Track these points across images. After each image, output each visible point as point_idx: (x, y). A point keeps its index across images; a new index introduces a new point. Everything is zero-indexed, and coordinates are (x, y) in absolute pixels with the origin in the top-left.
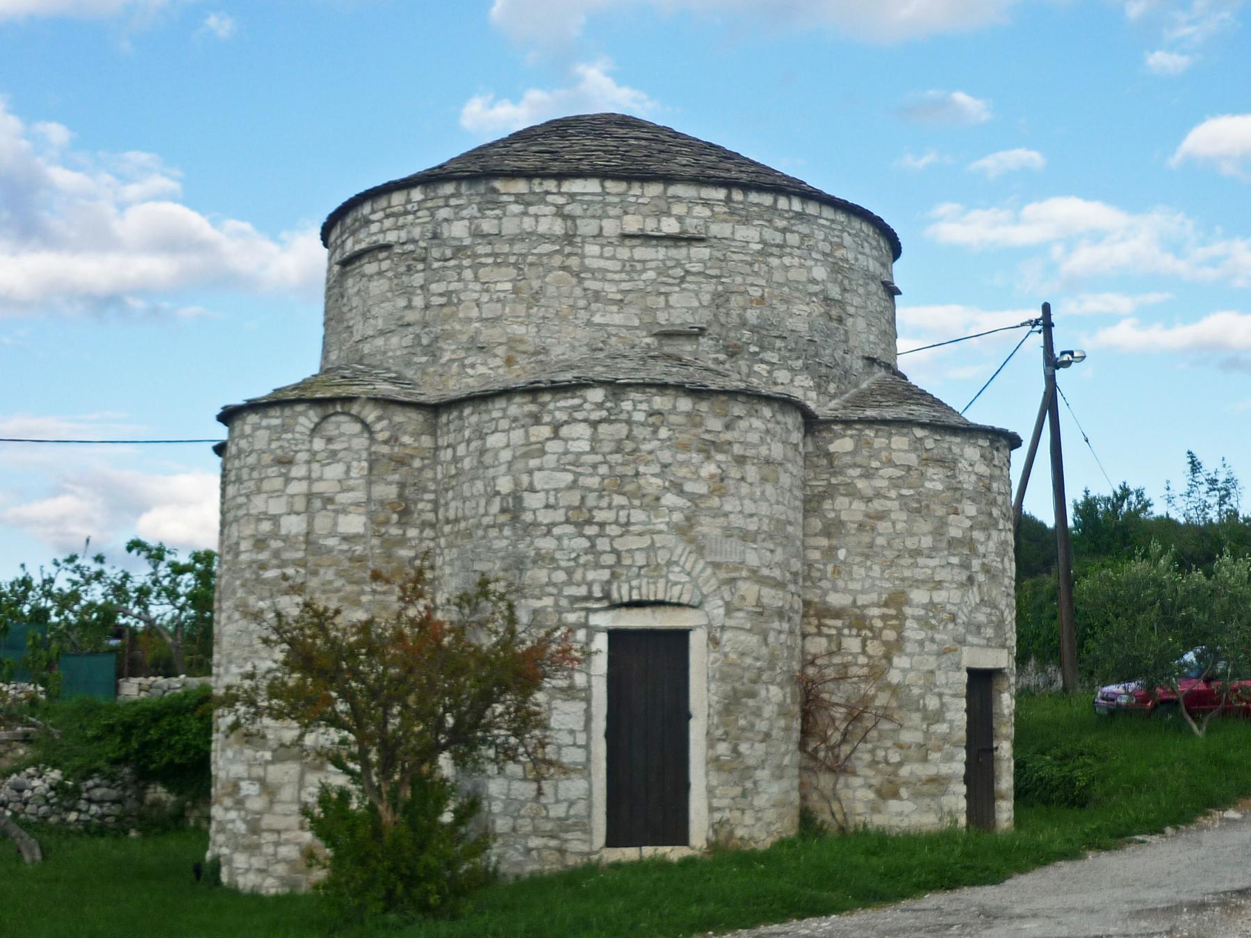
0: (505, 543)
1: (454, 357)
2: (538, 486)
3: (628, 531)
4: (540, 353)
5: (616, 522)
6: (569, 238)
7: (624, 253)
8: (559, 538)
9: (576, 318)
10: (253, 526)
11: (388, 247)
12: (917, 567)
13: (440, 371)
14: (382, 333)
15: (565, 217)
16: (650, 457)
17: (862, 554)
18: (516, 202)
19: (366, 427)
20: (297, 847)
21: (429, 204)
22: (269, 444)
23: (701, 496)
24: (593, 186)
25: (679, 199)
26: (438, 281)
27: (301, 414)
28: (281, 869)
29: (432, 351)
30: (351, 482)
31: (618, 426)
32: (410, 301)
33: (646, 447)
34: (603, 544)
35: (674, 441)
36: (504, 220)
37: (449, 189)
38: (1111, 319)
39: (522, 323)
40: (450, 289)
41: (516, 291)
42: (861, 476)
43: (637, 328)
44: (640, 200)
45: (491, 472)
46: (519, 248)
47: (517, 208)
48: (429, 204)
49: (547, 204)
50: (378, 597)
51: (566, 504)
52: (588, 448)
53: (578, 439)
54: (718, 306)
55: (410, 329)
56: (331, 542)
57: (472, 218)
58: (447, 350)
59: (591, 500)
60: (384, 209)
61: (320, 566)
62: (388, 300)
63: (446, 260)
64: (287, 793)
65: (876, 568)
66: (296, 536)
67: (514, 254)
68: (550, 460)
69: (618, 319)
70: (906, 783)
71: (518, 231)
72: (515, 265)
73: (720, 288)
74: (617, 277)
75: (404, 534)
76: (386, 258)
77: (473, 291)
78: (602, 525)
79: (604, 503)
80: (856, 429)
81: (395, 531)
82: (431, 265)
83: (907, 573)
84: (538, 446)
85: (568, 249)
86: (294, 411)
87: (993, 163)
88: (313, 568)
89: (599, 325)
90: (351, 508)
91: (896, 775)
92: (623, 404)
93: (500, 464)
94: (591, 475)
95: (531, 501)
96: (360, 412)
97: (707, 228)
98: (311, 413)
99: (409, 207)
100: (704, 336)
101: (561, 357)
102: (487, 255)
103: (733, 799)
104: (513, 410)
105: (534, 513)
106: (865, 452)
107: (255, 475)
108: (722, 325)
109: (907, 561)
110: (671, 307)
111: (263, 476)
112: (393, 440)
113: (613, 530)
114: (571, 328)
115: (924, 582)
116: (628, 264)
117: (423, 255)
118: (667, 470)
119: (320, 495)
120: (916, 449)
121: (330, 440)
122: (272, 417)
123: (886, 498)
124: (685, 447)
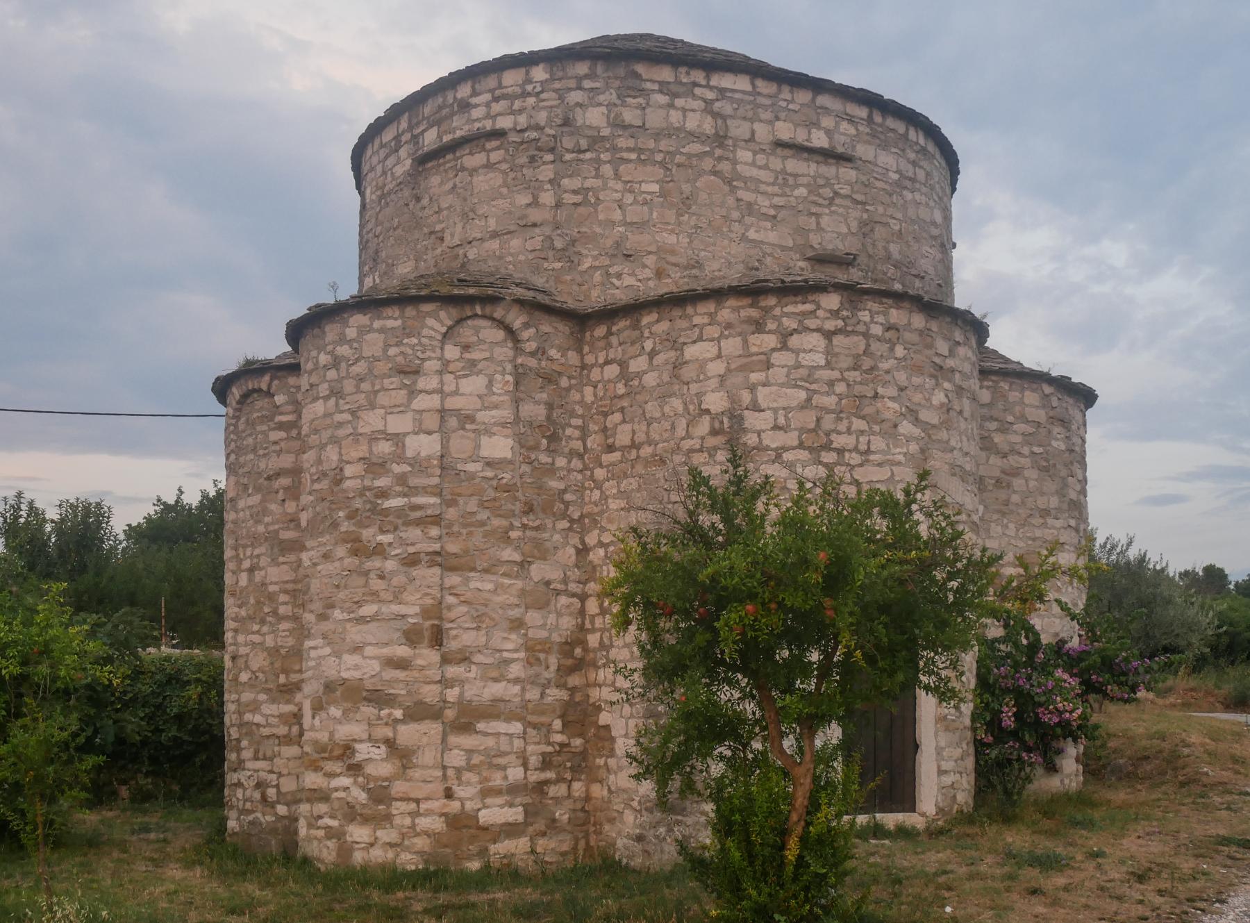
1: (597, 263)
2: (763, 403)
3: (867, 461)
4: (694, 267)
5: (856, 449)
6: (720, 139)
7: (776, 163)
9: (731, 231)
10: (365, 448)
11: (499, 134)
13: (579, 279)
14: (495, 235)
15: (716, 115)
16: (888, 377)
17: (999, 511)
18: (661, 92)
19: (510, 331)
20: (443, 819)
21: (557, 85)
22: (385, 351)
23: (934, 426)
26: (571, 176)
27: (428, 314)
28: (421, 843)
29: (568, 254)
30: (495, 398)
31: (856, 338)
32: (535, 198)
33: (884, 365)
35: (909, 362)
36: (648, 110)
39: (672, 231)
40: (585, 186)
41: (663, 194)
42: (997, 430)
43: (791, 249)
44: (791, 106)
45: (694, 388)
46: (664, 144)
47: (662, 99)
48: (557, 85)
49: (694, 97)
50: (528, 533)
51: (799, 425)
52: (823, 363)
53: (811, 351)
54: (865, 235)
55: (537, 230)
56: (472, 467)
57: (610, 105)
58: (587, 256)
59: (828, 422)
60: (492, 91)
61: (460, 495)
62: (503, 197)
64: (428, 757)
65: (1011, 526)
66: (429, 458)
67: (661, 151)
68: (778, 374)
69: (772, 237)
71: (664, 125)
72: (662, 164)
73: (865, 216)
74: (770, 189)
75: (553, 464)
76: (498, 148)
77: (611, 195)
78: (840, 451)
79: (842, 427)
80: (993, 381)
81: (544, 458)
83: (1038, 533)
84: (762, 357)
85: (718, 152)
86: (418, 311)
88: (449, 497)
89: (753, 241)
90: (495, 429)
92: (860, 314)
94: (828, 394)
95: (753, 420)
97: (854, 147)
98: (442, 314)
99: (529, 88)
100: (853, 267)
101: (716, 273)
102: (629, 150)
103: (956, 761)
104: (725, 314)
105: (759, 435)
106: (1000, 405)
107: (365, 386)
108: (870, 256)
109: (1037, 521)
110: (823, 229)
111: (377, 387)
112: (539, 353)
114: (726, 242)
116: (780, 177)
117: (552, 144)
118: (902, 394)
120: (1044, 407)
121: (466, 347)
122: (389, 318)
124: (918, 370)
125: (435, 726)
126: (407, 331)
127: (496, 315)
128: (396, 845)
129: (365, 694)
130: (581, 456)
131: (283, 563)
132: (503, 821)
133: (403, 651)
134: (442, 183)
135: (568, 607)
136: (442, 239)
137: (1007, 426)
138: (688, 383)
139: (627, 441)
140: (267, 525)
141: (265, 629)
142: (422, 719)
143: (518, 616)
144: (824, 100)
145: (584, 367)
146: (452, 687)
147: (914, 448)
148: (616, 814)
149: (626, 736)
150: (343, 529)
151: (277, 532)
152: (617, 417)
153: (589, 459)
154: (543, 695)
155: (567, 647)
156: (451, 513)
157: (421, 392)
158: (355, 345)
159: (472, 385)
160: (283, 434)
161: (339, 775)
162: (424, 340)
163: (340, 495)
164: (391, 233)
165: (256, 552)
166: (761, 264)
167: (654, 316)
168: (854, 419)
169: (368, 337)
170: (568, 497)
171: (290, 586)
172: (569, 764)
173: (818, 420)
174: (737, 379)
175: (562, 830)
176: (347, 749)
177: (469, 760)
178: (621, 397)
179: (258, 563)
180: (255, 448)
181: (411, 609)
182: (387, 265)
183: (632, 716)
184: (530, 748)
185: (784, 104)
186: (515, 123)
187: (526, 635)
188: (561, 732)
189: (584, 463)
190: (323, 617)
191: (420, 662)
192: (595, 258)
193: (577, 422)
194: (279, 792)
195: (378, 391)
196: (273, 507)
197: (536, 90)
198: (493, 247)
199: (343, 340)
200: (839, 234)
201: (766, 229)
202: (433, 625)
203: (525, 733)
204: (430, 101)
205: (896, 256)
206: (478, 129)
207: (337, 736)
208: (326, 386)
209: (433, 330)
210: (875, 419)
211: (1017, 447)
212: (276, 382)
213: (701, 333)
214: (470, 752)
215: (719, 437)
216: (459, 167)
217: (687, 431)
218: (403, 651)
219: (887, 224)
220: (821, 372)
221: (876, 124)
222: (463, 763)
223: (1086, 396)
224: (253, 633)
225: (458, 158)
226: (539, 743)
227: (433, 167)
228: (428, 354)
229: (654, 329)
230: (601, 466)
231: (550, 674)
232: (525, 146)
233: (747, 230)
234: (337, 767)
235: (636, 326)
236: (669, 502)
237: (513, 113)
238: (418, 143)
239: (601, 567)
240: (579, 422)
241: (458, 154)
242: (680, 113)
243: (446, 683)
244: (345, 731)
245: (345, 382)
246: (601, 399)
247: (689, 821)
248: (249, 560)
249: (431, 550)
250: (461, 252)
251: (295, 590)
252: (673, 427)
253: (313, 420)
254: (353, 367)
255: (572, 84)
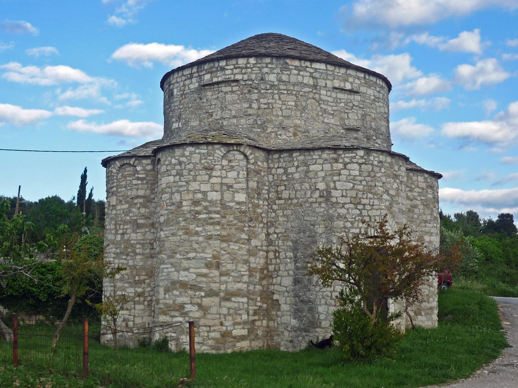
0: (322, 210)
1: (273, 130)
5: (369, 204)
6: (315, 86)
7: (334, 95)
8: (348, 209)
10: (192, 195)
11: (237, 81)
12: (426, 227)
13: (266, 135)
14: (235, 117)
15: (314, 78)
16: (379, 179)
18: (295, 69)
19: (246, 156)
21: (259, 66)
22: (200, 161)
23: (394, 196)
24: (322, 66)
25: (351, 75)
26: (263, 98)
27: (217, 149)
29: (263, 127)
32: (250, 105)
33: (378, 175)
34: (365, 213)
36: (291, 76)
37: (268, 60)
38: (76, 118)
39: (299, 119)
40: (269, 102)
41: (296, 106)
43: (339, 125)
45: (313, 180)
46: (296, 88)
47: (296, 72)
48: (259, 66)
50: (251, 229)
52: (358, 174)
53: (354, 170)
54: (363, 120)
55: (251, 117)
56: (232, 204)
58: (269, 127)
59: (360, 195)
60: (234, 65)
61: (227, 214)
63: (267, 90)
64: (214, 310)
66: (216, 201)
68: (343, 177)
69: (332, 121)
70: (424, 310)
71: (296, 81)
72: (295, 95)
73: (363, 113)
74: (332, 104)
75: (259, 203)
77: (278, 105)
78: (364, 205)
79: (365, 196)
81: (256, 201)
82: (260, 91)
83: (423, 229)
84: (338, 171)
85: (314, 91)
86: (213, 148)
87: (35, 51)
89: (326, 123)
90: (240, 191)
91: (420, 306)
92: (370, 157)
93: (318, 178)
94: (360, 185)
95: (334, 193)
96: (244, 151)
98: (222, 149)
99: (248, 66)
100: (360, 131)
102: (284, 90)
104: (325, 155)
105: (337, 199)
107: (192, 173)
109: (423, 225)
110: (349, 118)
111: (197, 174)
112: (255, 163)
113: (368, 207)
115: (428, 233)
118: (384, 185)
119: (226, 184)
120: (425, 182)
121: (230, 161)
122: (202, 149)
123: (417, 199)
124: (388, 176)
125: (217, 299)
126: (209, 154)
127: (241, 150)
128: (201, 343)
129: (189, 286)
130: (267, 200)
131: (139, 232)
132: (241, 334)
133: (205, 271)
134: (212, 95)
135: (262, 255)
136: (212, 115)
137: (412, 189)
138: (311, 179)
139: (287, 197)
140: (131, 217)
141: (129, 258)
142: (212, 296)
143: (247, 258)
144: (350, 72)
145: (269, 168)
146: (223, 284)
147: (387, 203)
148: (280, 333)
149: (286, 303)
150: (181, 225)
151: (136, 220)
152: (283, 188)
153: (270, 201)
154: (255, 288)
155: (262, 270)
156: (224, 221)
157: (213, 176)
158: (189, 158)
159: (232, 174)
160: (139, 182)
161: (177, 317)
162: (215, 158)
163: (181, 212)
164: (187, 109)
165: (125, 227)
166: (329, 131)
167: (298, 154)
168: (368, 194)
169: (194, 155)
170: (263, 215)
171: (142, 242)
172: (262, 314)
173: (357, 194)
174: (329, 178)
175: (259, 339)
176: (182, 306)
177: (229, 312)
178: (284, 181)
179: (126, 232)
180: (126, 186)
181: (209, 256)
182: (186, 121)
183: (288, 296)
184: (250, 307)
185: (336, 74)
186: (243, 78)
187: (249, 266)
188: (260, 302)
189: (268, 202)
190: (170, 257)
191: (211, 275)
192: (272, 128)
193: (266, 188)
194: (134, 324)
195: (197, 175)
196: (134, 210)
197: (251, 67)
198: (234, 121)
199: (183, 155)
200: (355, 119)
201: (330, 118)
202: (217, 262)
203: (248, 302)
204: (207, 64)
205: (374, 127)
206: (228, 78)
207: (177, 302)
208: (175, 171)
209: (219, 154)
210: (374, 194)
211: (416, 197)
212: (137, 161)
213: (316, 161)
214: (229, 309)
215: (322, 198)
216: (220, 90)
217: (311, 195)
218: (205, 271)
219: (370, 115)
220: (358, 177)
221: (367, 79)
222: (226, 313)
223: (440, 176)
224: (123, 259)
225: (220, 87)
226: (253, 306)
227: (208, 89)
228: (217, 163)
229: (298, 158)
230: (275, 204)
231: (257, 280)
232: (246, 86)
233: (324, 119)
234: (177, 314)
235: (291, 156)
236: (304, 220)
237: (242, 74)
238: (201, 78)
239: (275, 241)
240: (267, 188)
241: (220, 86)
242: (302, 77)
243: (221, 283)
244: (180, 300)
245: (184, 171)
246: (276, 180)
247: (311, 335)
248: (122, 230)
249: (216, 234)
250: (220, 122)
251: (143, 243)
252: (305, 193)
253: (169, 183)
254: (188, 166)
255: (264, 65)
